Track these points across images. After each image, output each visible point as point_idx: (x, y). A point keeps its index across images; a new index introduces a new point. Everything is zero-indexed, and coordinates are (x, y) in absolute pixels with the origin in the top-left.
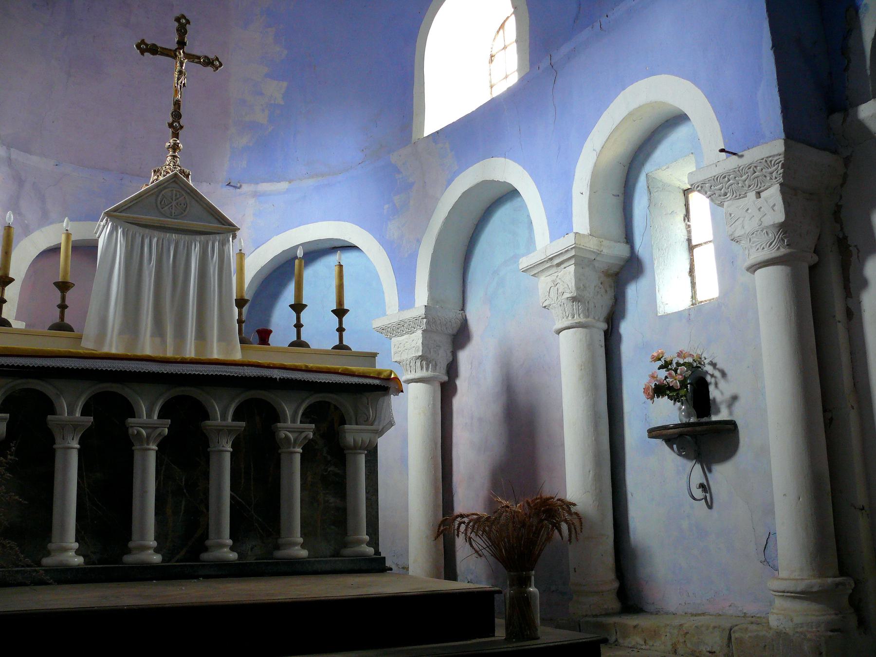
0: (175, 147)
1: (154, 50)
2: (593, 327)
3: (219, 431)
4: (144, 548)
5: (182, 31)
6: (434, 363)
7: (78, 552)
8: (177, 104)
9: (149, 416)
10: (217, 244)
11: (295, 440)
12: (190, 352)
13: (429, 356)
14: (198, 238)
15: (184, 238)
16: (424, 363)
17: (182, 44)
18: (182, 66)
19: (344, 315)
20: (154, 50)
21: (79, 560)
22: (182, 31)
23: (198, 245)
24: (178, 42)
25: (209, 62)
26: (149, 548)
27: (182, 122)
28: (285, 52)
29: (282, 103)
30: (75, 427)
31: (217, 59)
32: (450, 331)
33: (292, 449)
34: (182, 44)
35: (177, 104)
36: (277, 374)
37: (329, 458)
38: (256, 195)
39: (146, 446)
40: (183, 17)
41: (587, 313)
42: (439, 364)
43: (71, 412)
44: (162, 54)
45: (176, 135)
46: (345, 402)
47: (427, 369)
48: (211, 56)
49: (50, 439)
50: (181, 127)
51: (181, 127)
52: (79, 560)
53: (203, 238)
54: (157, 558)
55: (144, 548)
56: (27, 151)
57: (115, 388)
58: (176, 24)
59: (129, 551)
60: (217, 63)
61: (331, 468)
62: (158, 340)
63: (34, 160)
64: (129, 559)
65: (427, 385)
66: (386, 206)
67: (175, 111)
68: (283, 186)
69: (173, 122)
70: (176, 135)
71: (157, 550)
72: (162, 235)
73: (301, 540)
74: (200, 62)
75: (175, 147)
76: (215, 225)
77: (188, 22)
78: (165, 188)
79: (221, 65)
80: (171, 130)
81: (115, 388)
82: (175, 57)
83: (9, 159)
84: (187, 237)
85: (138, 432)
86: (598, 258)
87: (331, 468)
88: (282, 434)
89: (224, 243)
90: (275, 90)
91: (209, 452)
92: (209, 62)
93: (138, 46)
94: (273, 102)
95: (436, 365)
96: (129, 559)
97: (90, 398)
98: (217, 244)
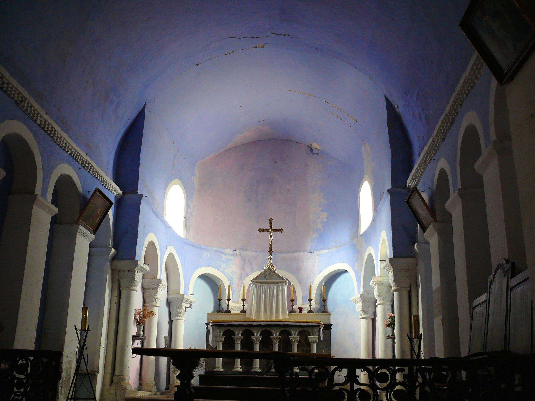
0: (270, 258)
1: (263, 230)
2: (385, 304)
3: (274, 338)
4: (256, 368)
5: (271, 223)
6: (367, 312)
7: (241, 368)
8: (271, 245)
9: (257, 335)
10: (281, 286)
11: (294, 341)
12: (274, 318)
13: (365, 310)
14: (276, 285)
15: (272, 286)
16: (364, 312)
17: (271, 227)
18: (271, 234)
19: (325, 301)
20: (263, 230)
21: (241, 370)
22: (271, 223)
23: (276, 286)
24: (270, 227)
25: (279, 230)
26: (258, 368)
27: (272, 250)
28: (326, 202)
29: (326, 220)
30: (239, 338)
31: (282, 229)
32: (373, 301)
33: (294, 343)
34: (271, 227)
35: (271, 245)
36: (288, 323)
37: (305, 345)
38: (318, 255)
39: (256, 343)
40: (271, 218)
41: (383, 300)
42: (369, 313)
43: (238, 335)
44: (265, 231)
45: (271, 254)
46: (310, 330)
47: (365, 314)
48: (280, 228)
49: (234, 341)
50: (272, 252)
51: (272, 252)
52: (241, 370)
53: (277, 284)
54: (259, 370)
55: (256, 368)
56: (246, 250)
57: (249, 328)
58: (269, 221)
59: (253, 368)
60: (282, 230)
61: (306, 348)
62: (265, 314)
63: (248, 253)
64: (252, 370)
65: (366, 320)
66: (354, 258)
67: (270, 247)
68: (326, 251)
69: (270, 251)
70: (271, 254)
71: (259, 369)
72: (266, 285)
73: (259, 367)
74: (276, 231)
75: (270, 258)
76: (280, 281)
77: (272, 220)
78: (266, 272)
79: (283, 230)
80: (269, 253)
81: (249, 328)
82: (269, 232)
83: (240, 254)
84: (273, 285)
85: (254, 339)
86: (384, 283)
87: (306, 348)
88: (291, 339)
89: (283, 285)
90: (324, 216)
91: (272, 344)
92: (279, 230)
93: (259, 230)
94: (323, 220)
95: (368, 313)
96: (252, 370)
97: (243, 331)
98: (281, 286)
